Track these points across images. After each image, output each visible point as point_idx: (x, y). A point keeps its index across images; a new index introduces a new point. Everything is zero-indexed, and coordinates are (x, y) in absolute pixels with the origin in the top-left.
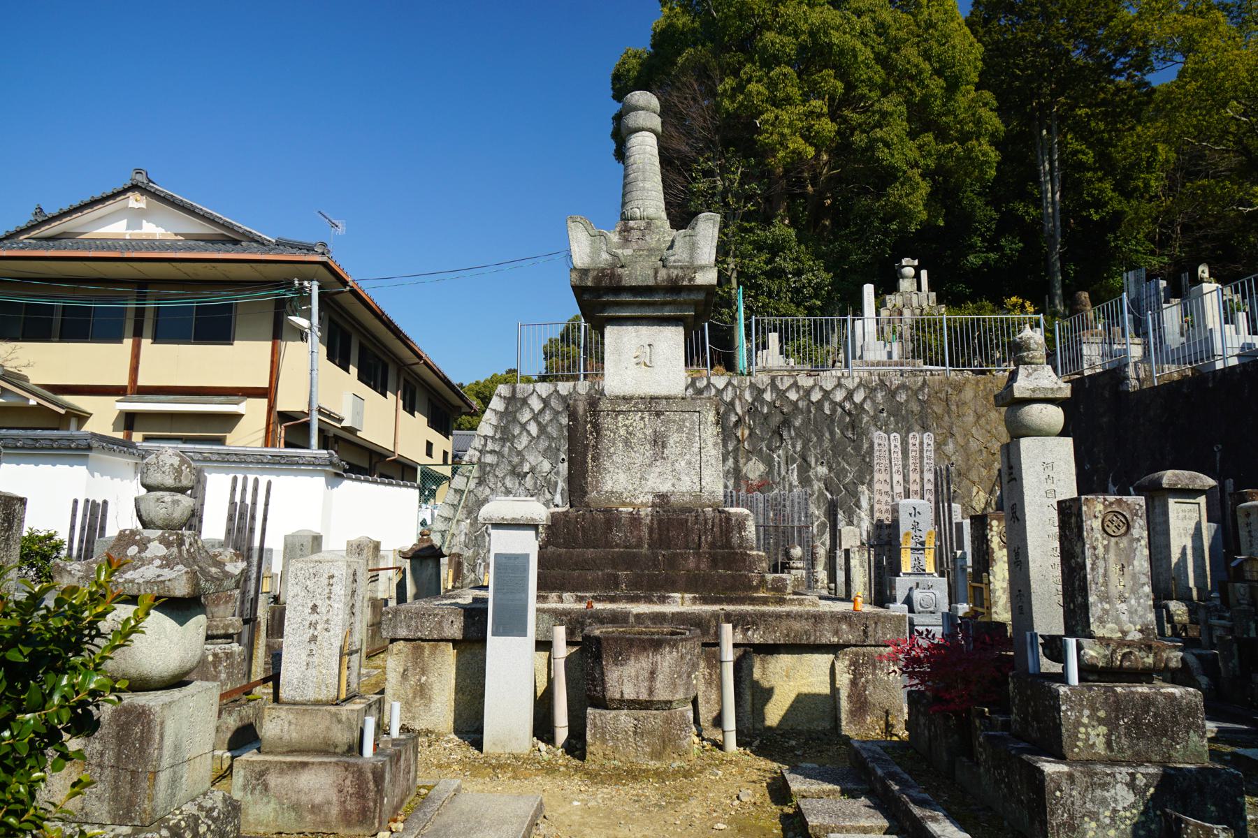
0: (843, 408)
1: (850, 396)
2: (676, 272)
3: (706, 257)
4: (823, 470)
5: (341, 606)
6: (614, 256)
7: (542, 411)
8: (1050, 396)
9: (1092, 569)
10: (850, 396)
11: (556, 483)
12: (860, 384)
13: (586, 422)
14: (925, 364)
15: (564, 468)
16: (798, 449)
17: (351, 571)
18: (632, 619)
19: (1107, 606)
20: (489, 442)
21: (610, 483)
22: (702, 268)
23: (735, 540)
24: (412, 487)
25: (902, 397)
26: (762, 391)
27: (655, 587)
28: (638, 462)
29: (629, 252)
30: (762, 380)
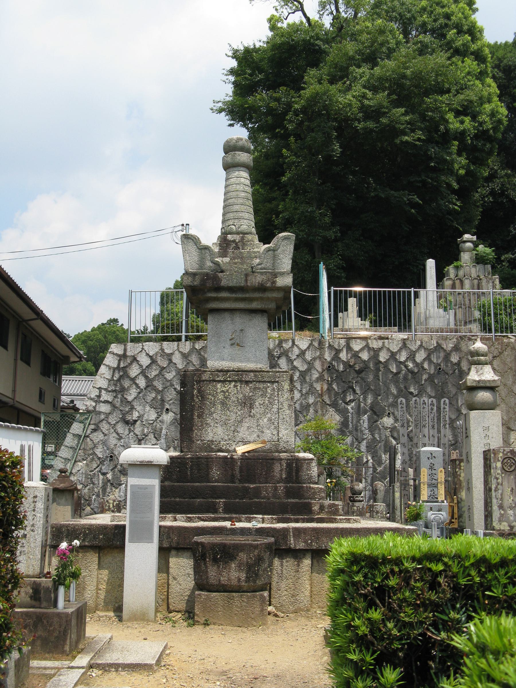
0: (406, 367)
1: (412, 356)
5: (41, 515)
6: (217, 264)
8: (488, 385)
9: (495, 491)
10: (412, 356)
11: (161, 429)
12: (421, 346)
17: (47, 493)
19: (502, 512)
20: (103, 392)
21: (211, 434)
24: (37, 431)
29: (227, 260)
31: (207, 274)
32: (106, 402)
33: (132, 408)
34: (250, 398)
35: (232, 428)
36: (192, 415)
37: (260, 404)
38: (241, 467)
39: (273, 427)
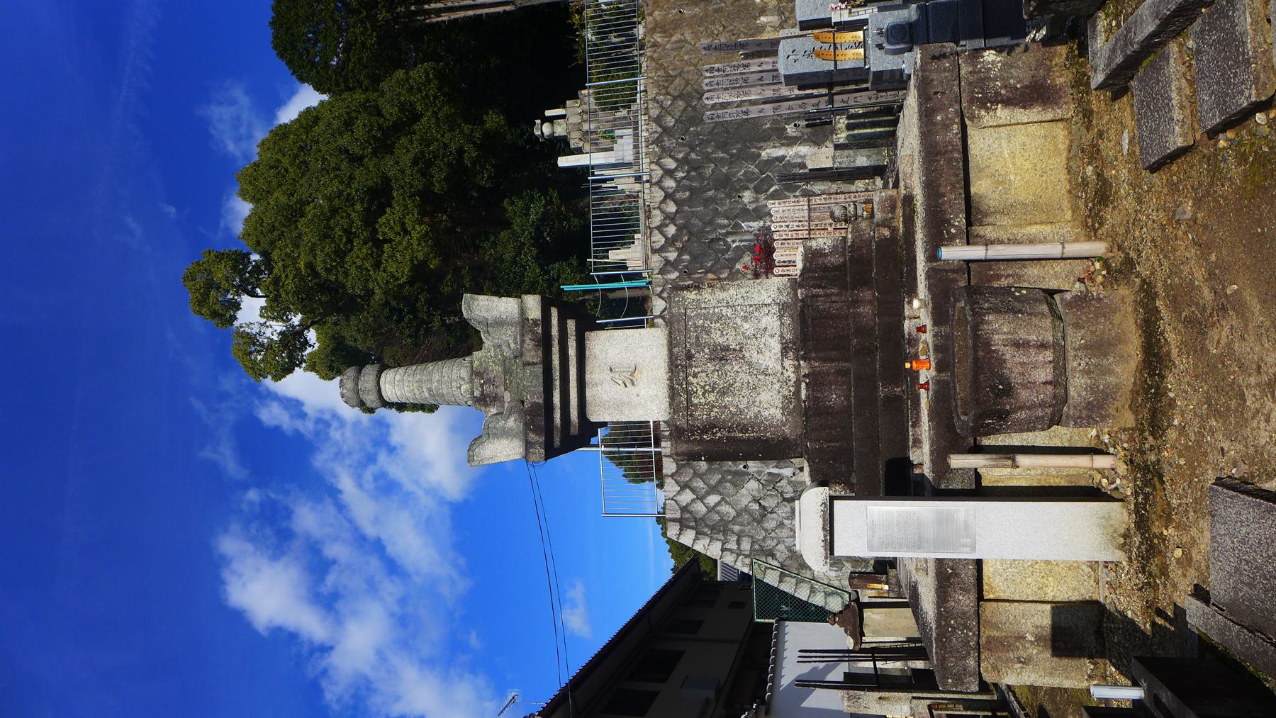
1: (669, 173)
2: (528, 341)
3: (510, 309)
4: (747, 196)
7: (693, 490)
10: (669, 173)
11: (770, 474)
12: (658, 163)
13: (702, 440)
14: (635, 101)
15: (753, 466)
16: (726, 222)
18: (945, 376)
21: (772, 411)
22: (522, 311)
23: (835, 260)
25: (670, 122)
26: (667, 262)
27: (896, 345)
28: (746, 378)
29: (507, 396)
30: (656, 261)
31: (526, 425)
32: (738, 543)
33: (746, 509)
34: (713, 351)
35: (762, 377)
36: (741, 440)
37: (722, 335)
38: (825, 360)
39: (756, 314)
